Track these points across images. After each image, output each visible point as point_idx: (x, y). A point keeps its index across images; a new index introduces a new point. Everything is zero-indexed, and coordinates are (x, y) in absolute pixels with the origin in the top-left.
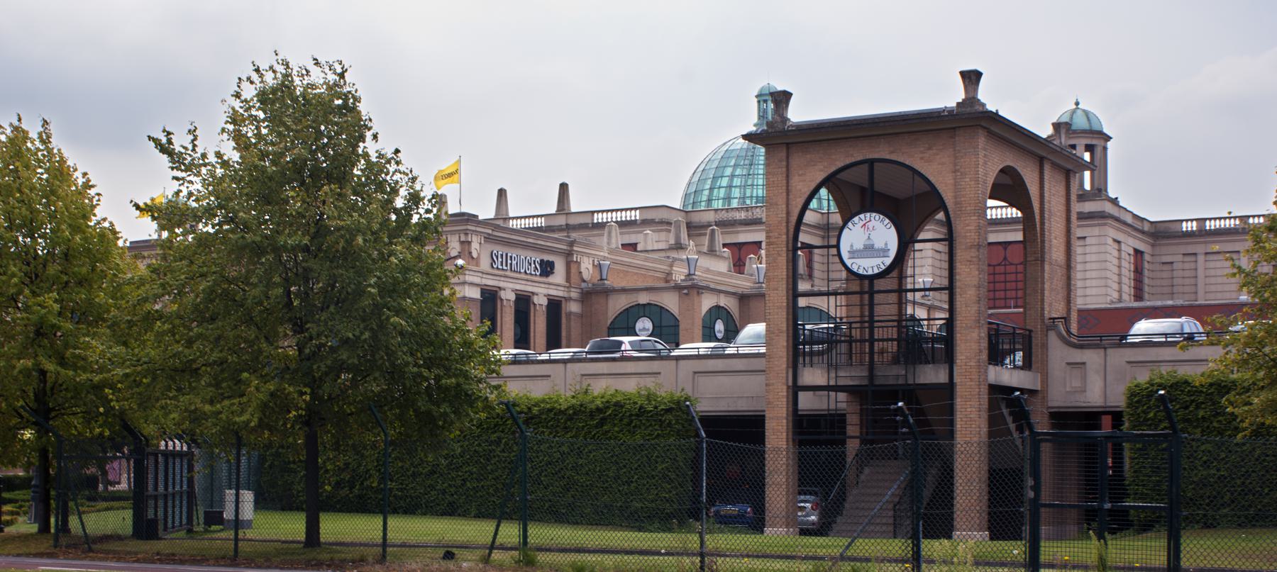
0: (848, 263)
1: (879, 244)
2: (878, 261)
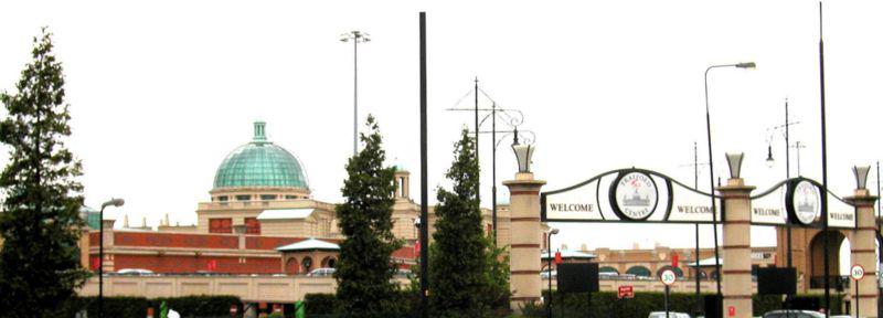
0: (622, 208)
1: (643, 197)
2: (642, 208)
